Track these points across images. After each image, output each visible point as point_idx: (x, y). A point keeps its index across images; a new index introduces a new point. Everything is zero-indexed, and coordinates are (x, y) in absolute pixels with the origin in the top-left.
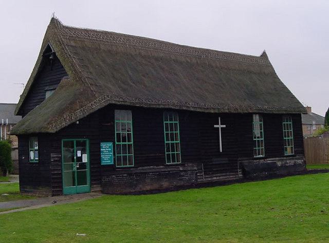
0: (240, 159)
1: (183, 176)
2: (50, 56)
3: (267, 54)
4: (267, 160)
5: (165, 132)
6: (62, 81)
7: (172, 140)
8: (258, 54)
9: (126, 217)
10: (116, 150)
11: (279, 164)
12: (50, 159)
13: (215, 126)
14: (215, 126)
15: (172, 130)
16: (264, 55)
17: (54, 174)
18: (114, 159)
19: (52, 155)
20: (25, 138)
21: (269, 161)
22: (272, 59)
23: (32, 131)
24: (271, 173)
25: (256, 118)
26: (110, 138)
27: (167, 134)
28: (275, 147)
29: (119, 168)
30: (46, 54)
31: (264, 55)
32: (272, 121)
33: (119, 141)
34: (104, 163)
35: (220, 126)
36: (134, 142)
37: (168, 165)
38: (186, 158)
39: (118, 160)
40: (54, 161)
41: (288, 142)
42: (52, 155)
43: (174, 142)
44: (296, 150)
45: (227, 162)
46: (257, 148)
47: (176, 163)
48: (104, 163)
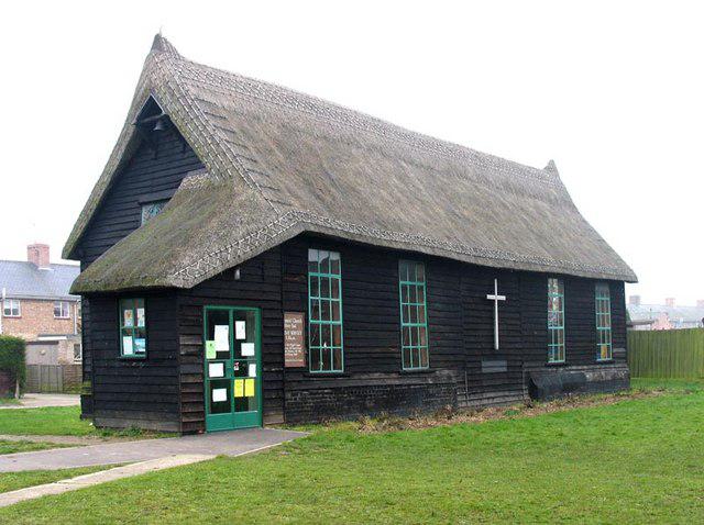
0: (526, 364)
1: (433, 395)
2: (154, 123)
3: (558, 167)
4: (371, 376)
5: (401, 304)
6: (185, 180)
7: (326, 316)
8: (540, 165)
9: (561, 435)
10: (310, 335)
11: (589, 376)
12: (177, 350)
13: (489, 297)
14: (489, 297)
15: (413, 300)
16: (551, 168)
17: (185, 385)
18: (307, 355)
19: (183, 340)
20: (101, 306)
21: (573, 370)
22: (566, 178)
23: (125, 285)
24: (572, 388)
25: (553, 286)
26: (300, 306)
27: (405, 308)
28: (582, 345)
29: (315, 376)
30: (146, 120)
31: (551, 168)
32: (579, 288)
33: (315, 317)
34: (288, 362)
35: (496, 297)
36: (344, 320)
37: (406, 373)
38: (438, 356)
39: (313, 357)
40: (188, 355)
41: (556, 335)
42: (183, 340)
43: (331, 322)
44: (615, 350)
45: (505, 369)
46: (411, 347)
47: (420, 368)
48: (288, 362)
